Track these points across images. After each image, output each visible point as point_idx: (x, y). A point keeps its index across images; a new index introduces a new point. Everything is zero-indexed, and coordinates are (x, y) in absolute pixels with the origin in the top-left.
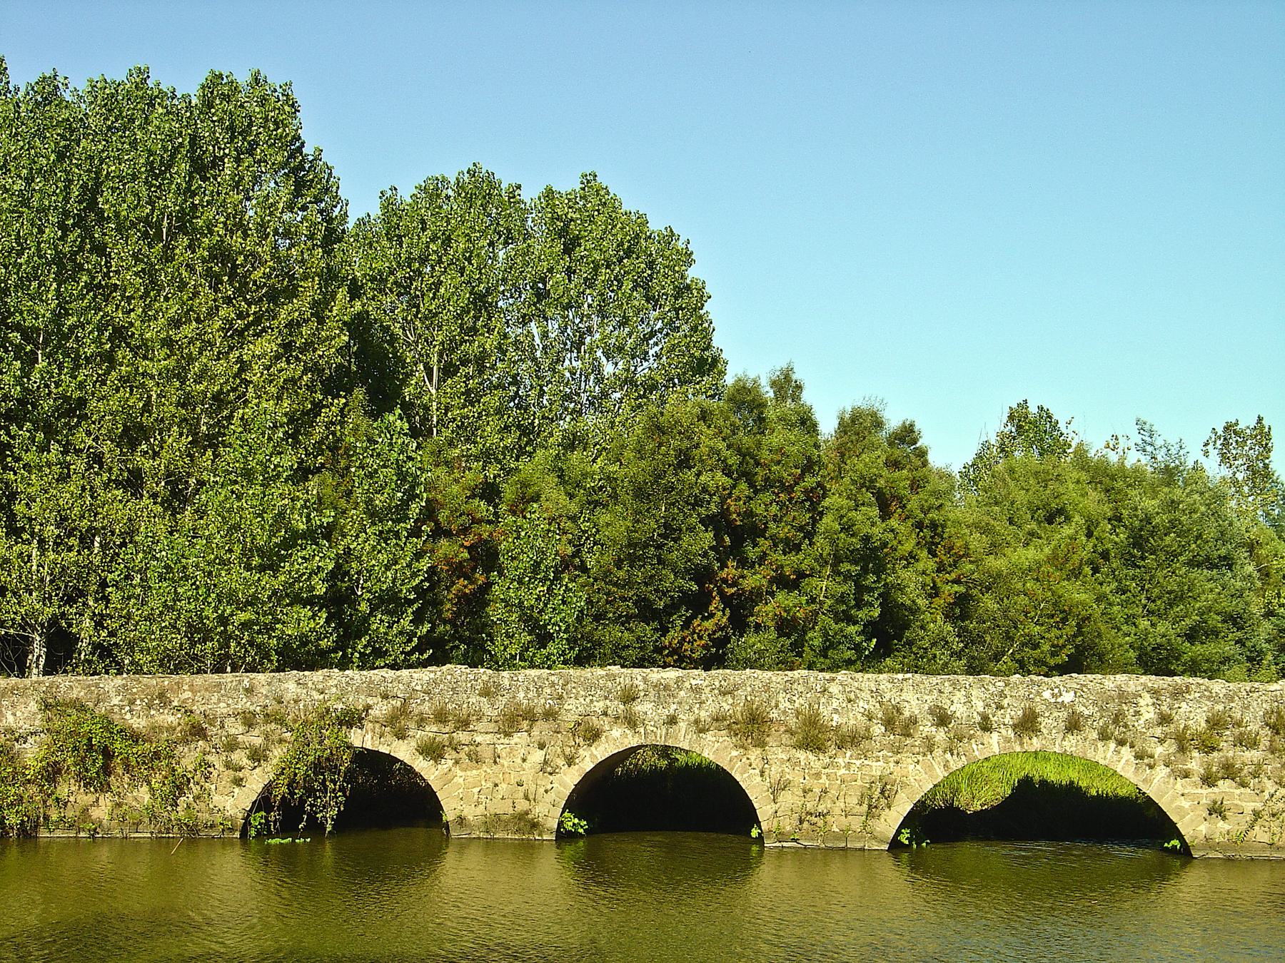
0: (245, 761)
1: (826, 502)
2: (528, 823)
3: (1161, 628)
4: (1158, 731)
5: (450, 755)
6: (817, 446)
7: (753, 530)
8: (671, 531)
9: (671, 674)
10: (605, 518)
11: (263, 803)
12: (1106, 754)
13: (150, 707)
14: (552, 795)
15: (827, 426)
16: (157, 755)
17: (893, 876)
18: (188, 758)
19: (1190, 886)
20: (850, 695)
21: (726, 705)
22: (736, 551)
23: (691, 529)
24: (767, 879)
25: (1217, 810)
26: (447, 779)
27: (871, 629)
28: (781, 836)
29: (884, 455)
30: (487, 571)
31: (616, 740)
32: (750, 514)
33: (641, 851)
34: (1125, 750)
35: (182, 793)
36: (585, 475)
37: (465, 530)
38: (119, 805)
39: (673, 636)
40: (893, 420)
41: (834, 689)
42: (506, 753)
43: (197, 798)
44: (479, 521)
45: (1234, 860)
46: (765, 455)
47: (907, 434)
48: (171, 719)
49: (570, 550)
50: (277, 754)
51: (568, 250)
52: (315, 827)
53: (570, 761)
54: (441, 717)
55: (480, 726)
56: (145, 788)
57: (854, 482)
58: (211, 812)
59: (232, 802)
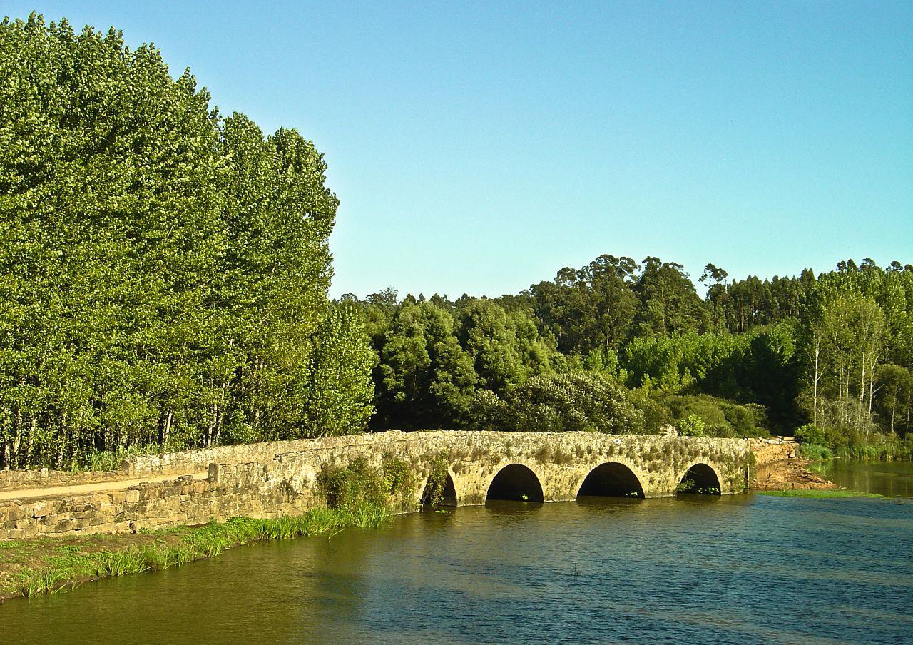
17: (578, 509)
19: (645, 505)
20: (568, 441)
34: (632, 460)
53: (491, 472)
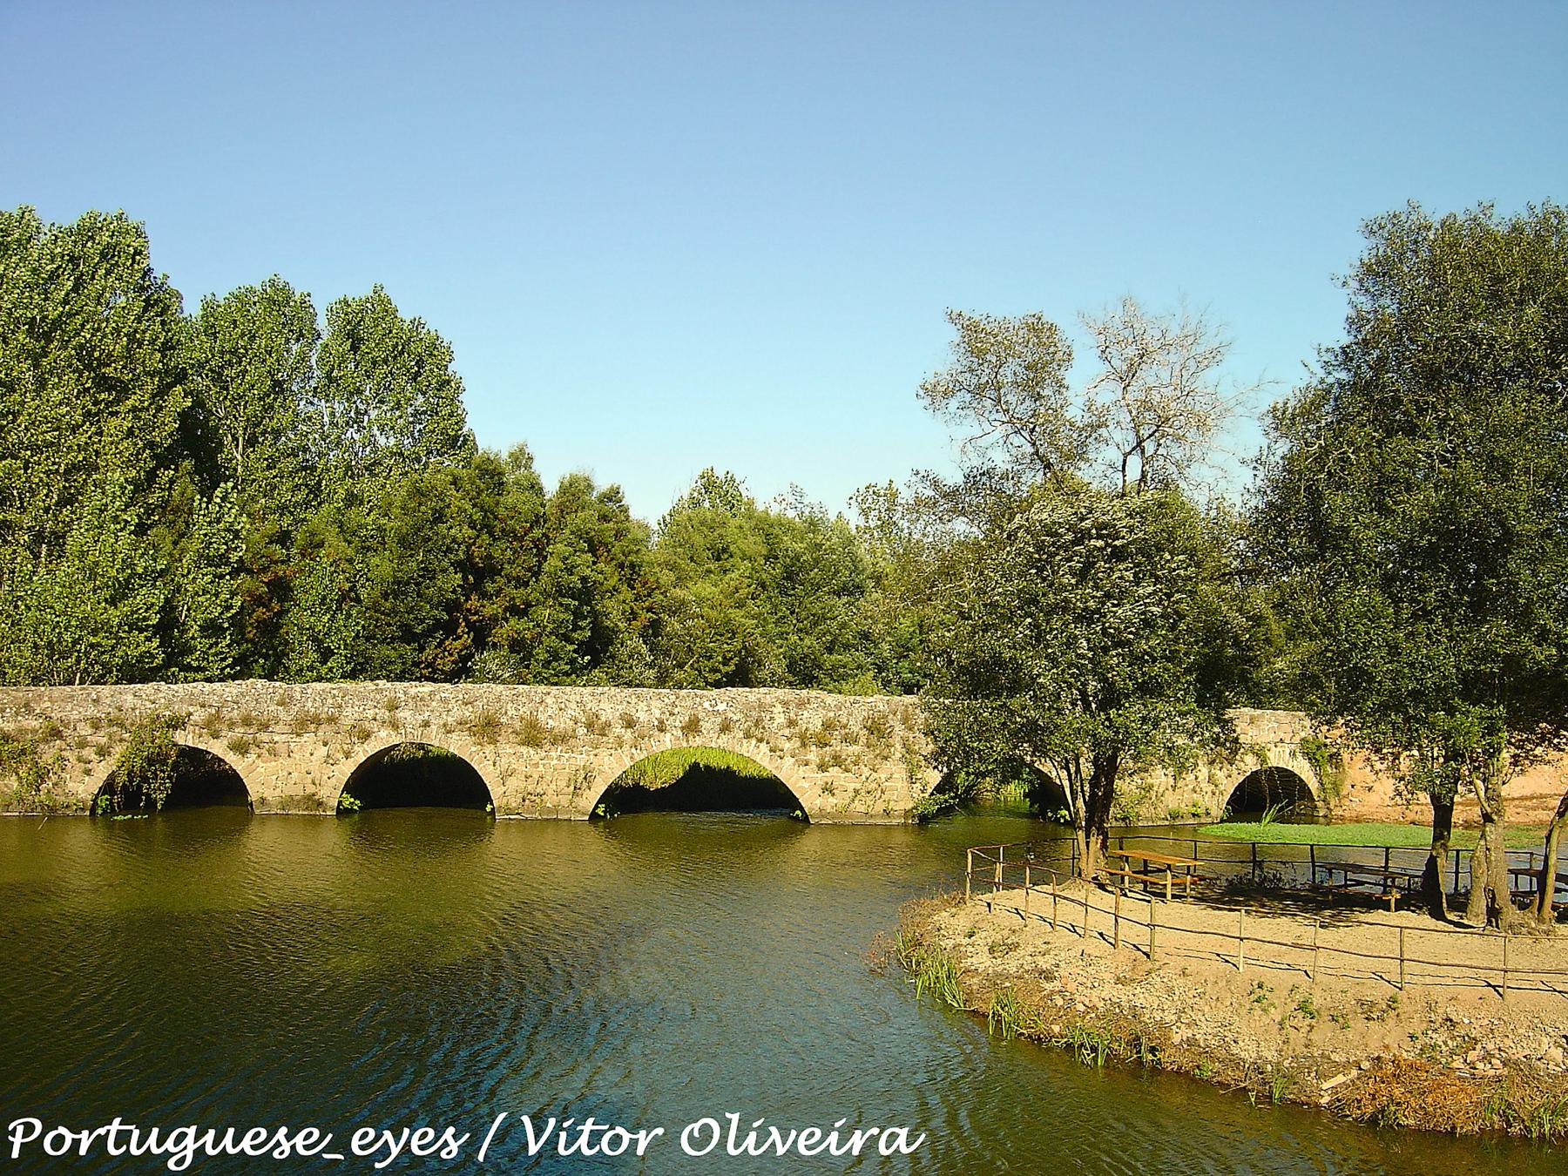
0: (93, 756)
1: (550, 549)
2: (314, 802)
3: (807, 642)
4: (787, 732)
5: (254, 750)
6: (543, 505)
7: (490, 570)
8: (428, 573)
9: (427, 687)
10: (376, 560)
11: (108, 787)
12: (749, 748)
13: (17, 714)
14: (333, 780)
15: (551, 486)
16: (23, 752)
18: (48, 753)
19: (809, 844)
20: (560, 704)
21: (467, 712)
22: (477, 588)
23: (444, 571)
24: (500, 845)
25: (828, 789)
26: (251, 769)
27: (584, 648)
28: (509, 811)
29: (596, 518)
30: (281, 601)
31: (383, 739)
32: (490, 557)
33: (403, 820)
34: (763, 746)
35: (43, 781)
36: (360, 526)
37: (264, 570)
39: (429, 653)
40: (602, 484)
41: (549, 700)
42: (299, 746)
43: (55, 784)
44: (276, 562)
45: (841, 827)
46: (502, 512)
47: (613, 496)
49: (347, 586)
50: (118, 750)
51: (355, 348)
52: (151, 804)
54: (247, 722)
55: (277, 729)
56: (14, 777)
57: (572, 533)
59: (83, 787)
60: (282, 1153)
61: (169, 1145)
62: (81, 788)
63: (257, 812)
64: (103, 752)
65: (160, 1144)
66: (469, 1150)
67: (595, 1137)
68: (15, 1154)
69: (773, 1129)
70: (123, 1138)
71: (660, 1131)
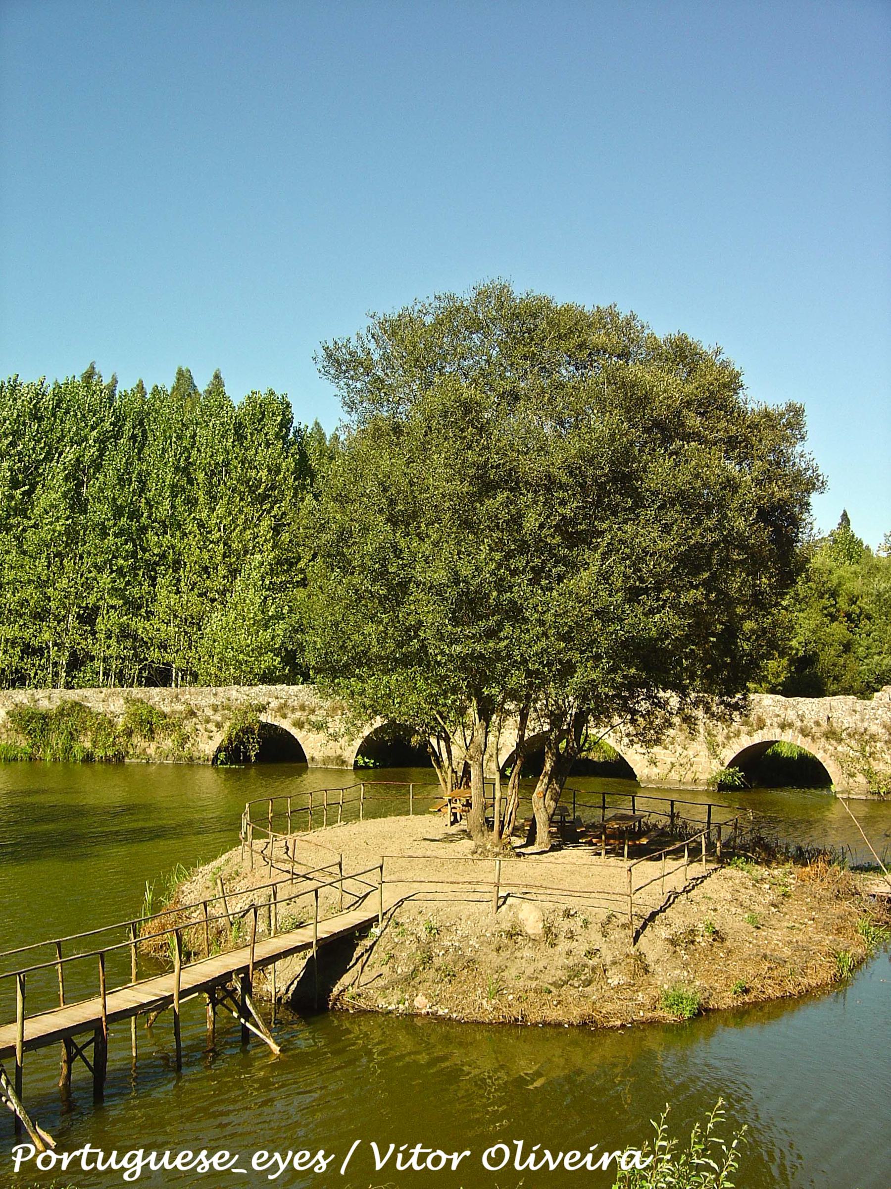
0: (214, 729)
35: (186, 743)
38: (158, 748)
48: (180, 707)
52: (247, 759)
54: (303, 708)
58: (199, 751)
59: (208, 745)
60: (203, 1168)
61: (124, 1163)
62: (207, 747)
63: (309, 766)
64: (219, 726)
65: (117, 1162)
66: (334, 1167)
67: (422, 1158)
68: (17, 1169)
69: (547, 1152)
70: (92, 1158)
71: (467, 1153)
